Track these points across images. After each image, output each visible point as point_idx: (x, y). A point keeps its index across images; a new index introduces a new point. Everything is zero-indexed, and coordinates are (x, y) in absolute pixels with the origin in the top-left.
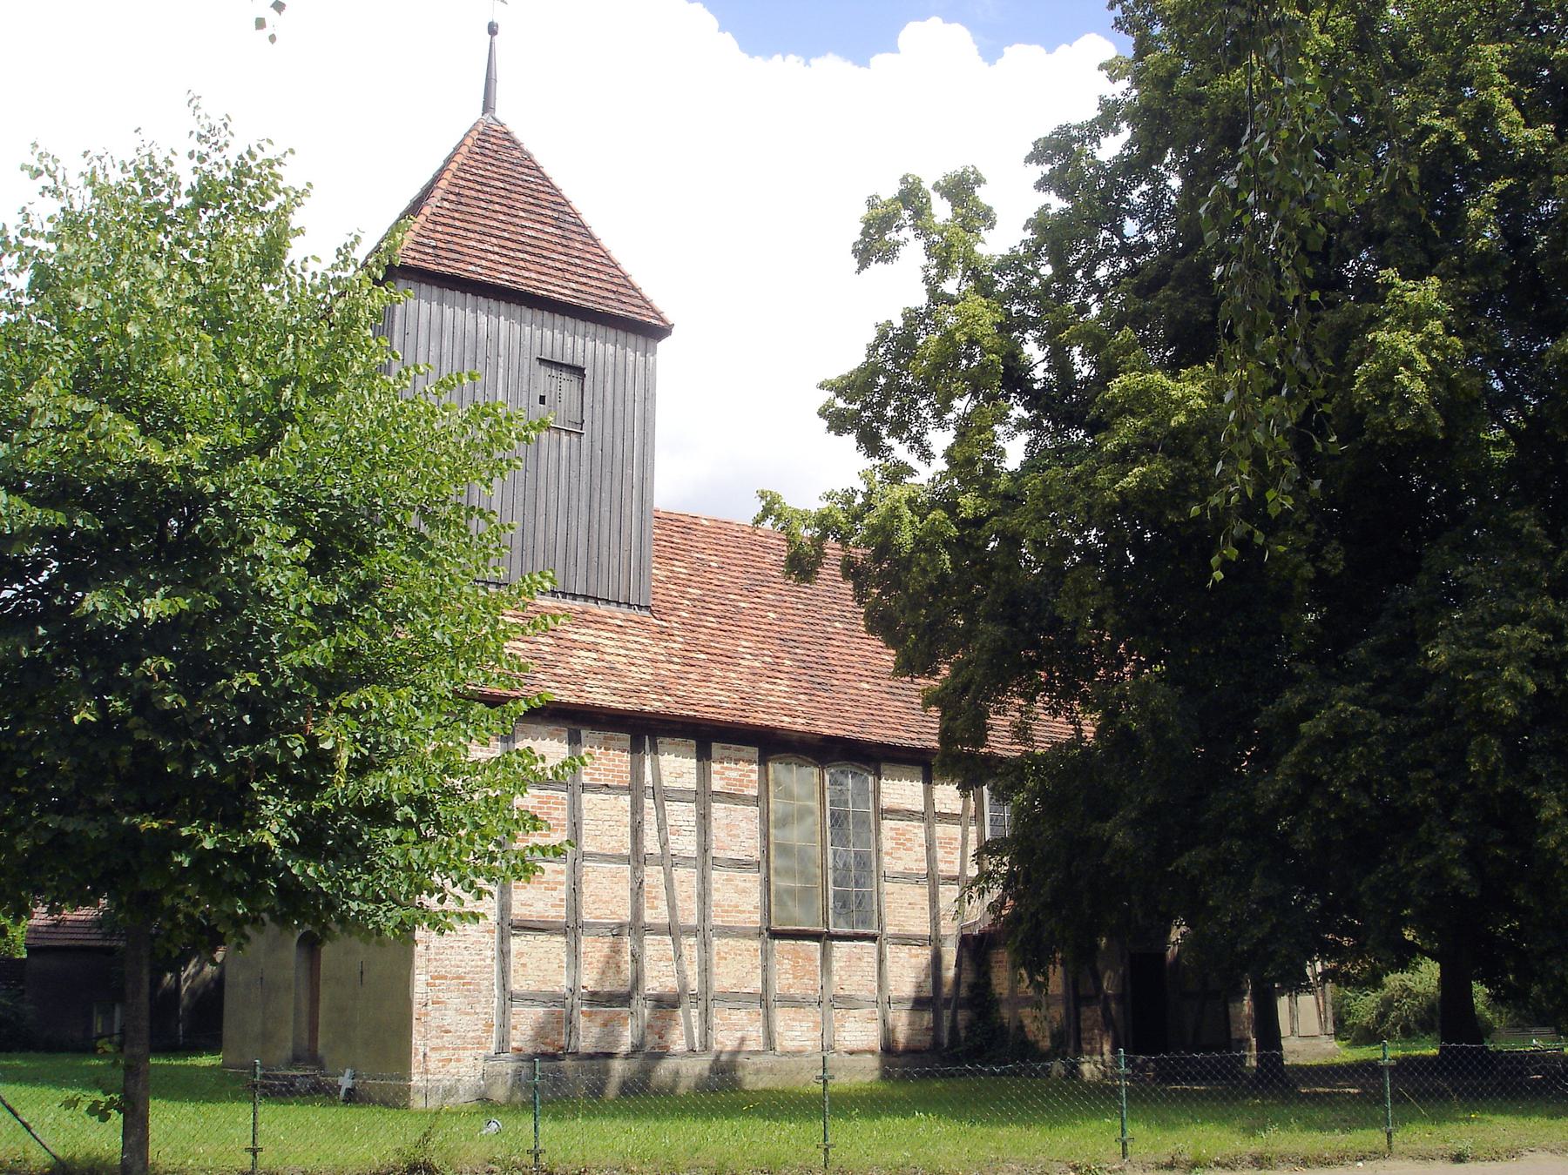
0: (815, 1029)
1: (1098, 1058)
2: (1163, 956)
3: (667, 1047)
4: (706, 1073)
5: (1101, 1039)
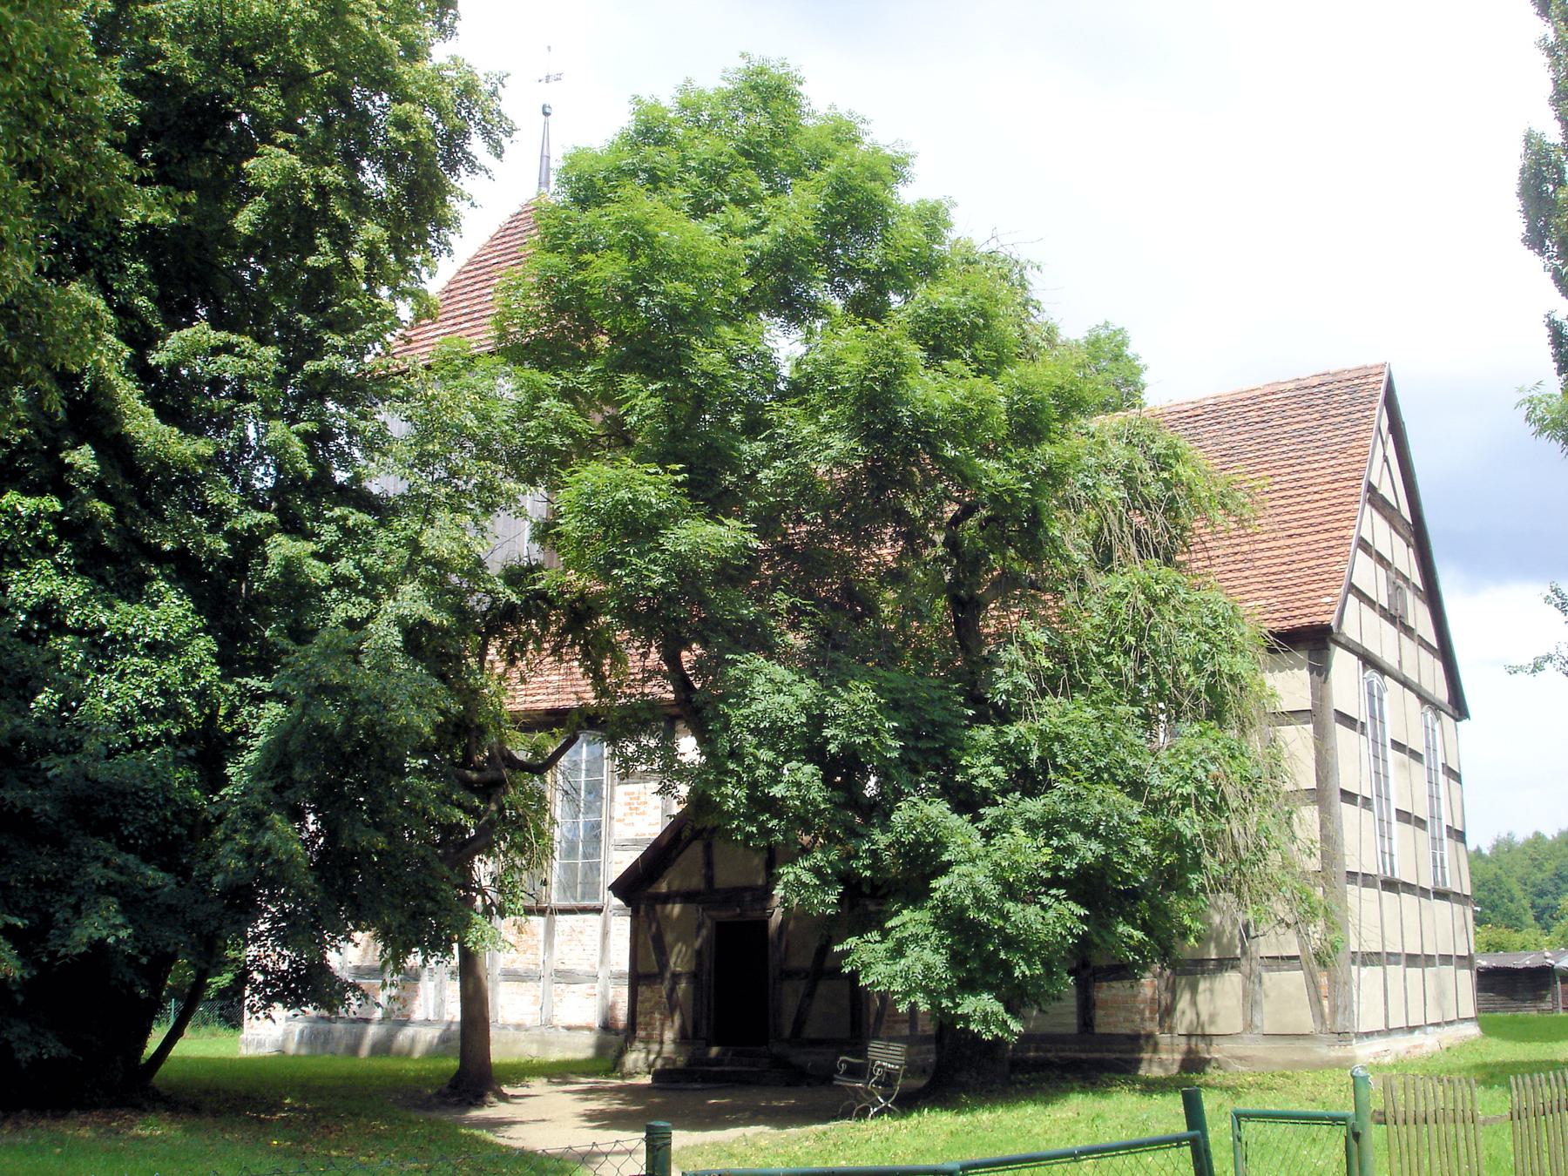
0: (535, 1003)
1: (655, 1047)
2: (764, 923)
3: (408, 1016)
4: (436, 1041)
5: (662, 1025)
